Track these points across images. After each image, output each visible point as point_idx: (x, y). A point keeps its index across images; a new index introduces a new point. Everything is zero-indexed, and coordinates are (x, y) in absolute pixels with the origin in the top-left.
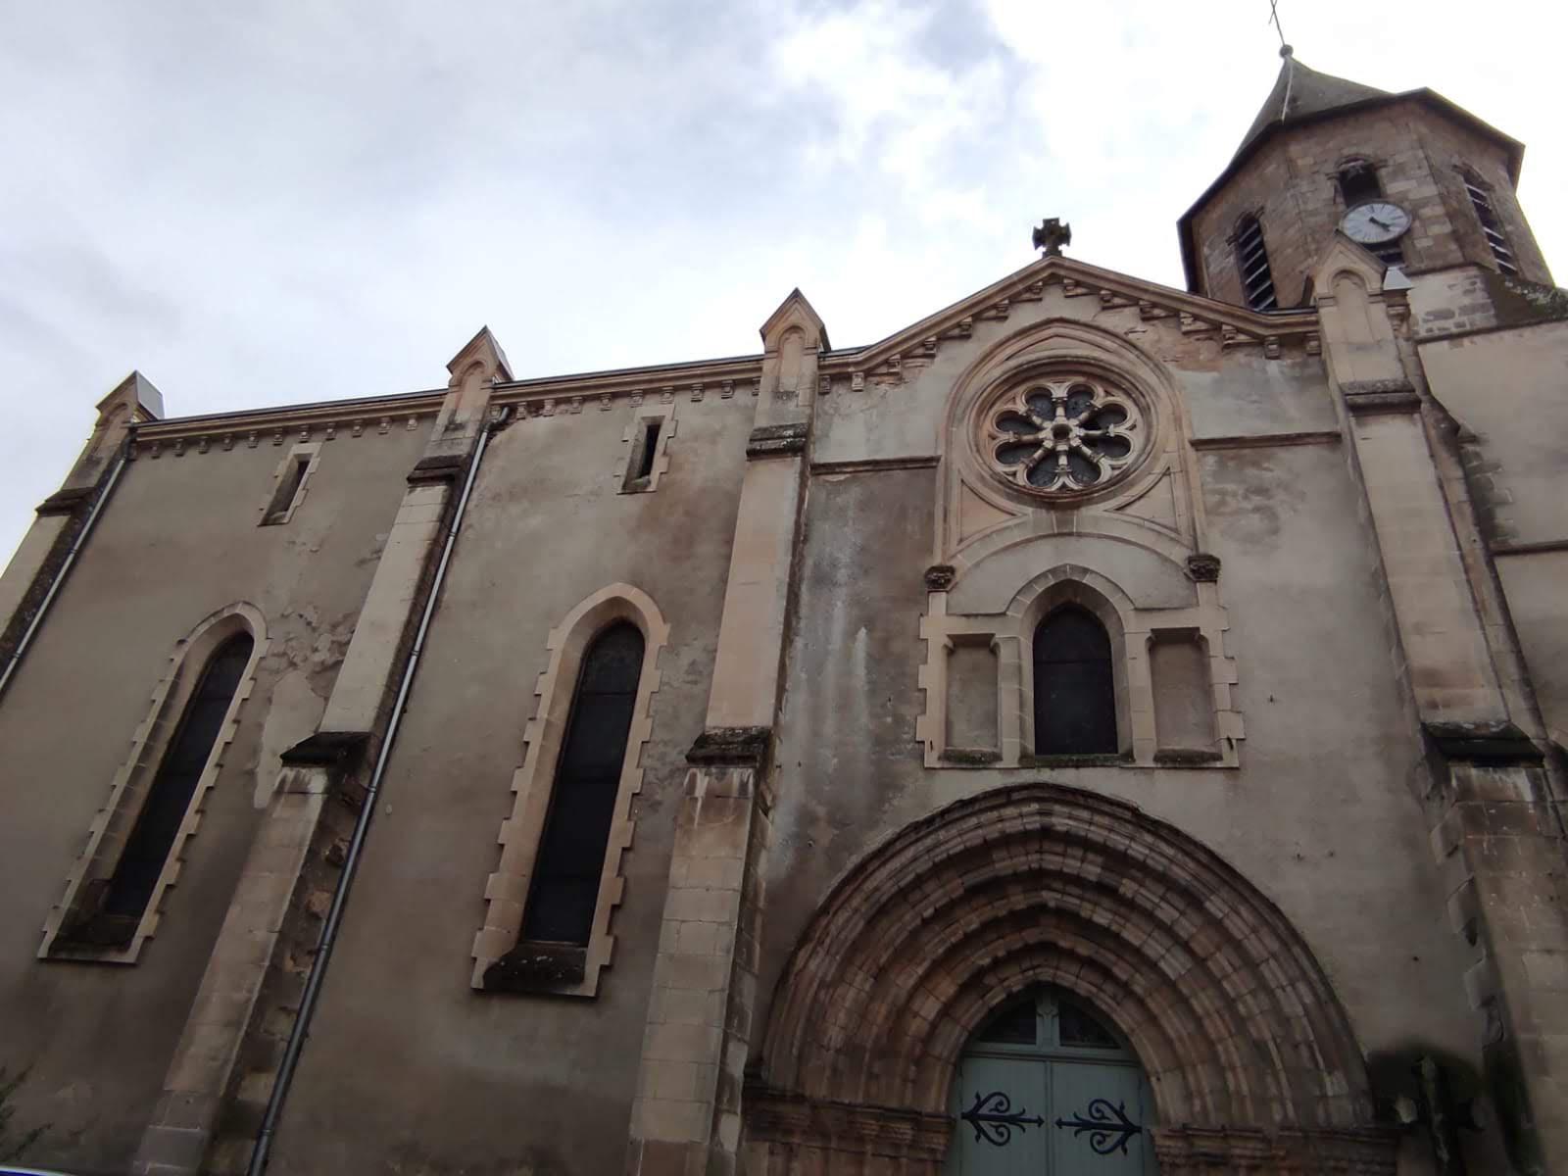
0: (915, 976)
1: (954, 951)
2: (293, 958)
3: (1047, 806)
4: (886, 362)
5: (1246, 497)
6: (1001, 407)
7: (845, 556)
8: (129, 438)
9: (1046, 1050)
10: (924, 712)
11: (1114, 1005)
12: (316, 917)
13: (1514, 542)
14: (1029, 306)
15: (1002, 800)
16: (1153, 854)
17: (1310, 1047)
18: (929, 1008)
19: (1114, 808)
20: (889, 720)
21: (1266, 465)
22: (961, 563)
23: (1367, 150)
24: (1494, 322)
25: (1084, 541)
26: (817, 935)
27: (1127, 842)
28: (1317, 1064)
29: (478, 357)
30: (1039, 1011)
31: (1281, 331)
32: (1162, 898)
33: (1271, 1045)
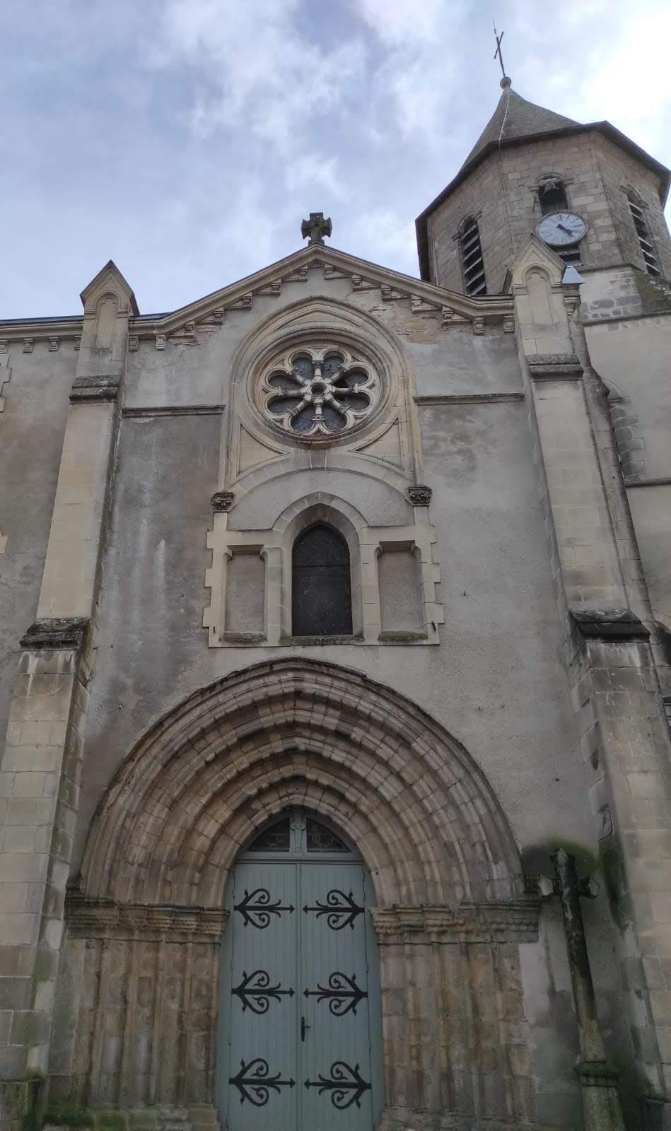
3: (299, 675)
4: (184, 327)
6: (273, 367)
7: (149, 484)
9: (298, 855)
11: (346, 820)
13: (643, 478)
14: (297, 285)
15: (266, 670)
16: (376, 709)
17: (483, 845)
18: (210, 828)
23: (559, 170)
24: (639, 312)
32: (382, 741)
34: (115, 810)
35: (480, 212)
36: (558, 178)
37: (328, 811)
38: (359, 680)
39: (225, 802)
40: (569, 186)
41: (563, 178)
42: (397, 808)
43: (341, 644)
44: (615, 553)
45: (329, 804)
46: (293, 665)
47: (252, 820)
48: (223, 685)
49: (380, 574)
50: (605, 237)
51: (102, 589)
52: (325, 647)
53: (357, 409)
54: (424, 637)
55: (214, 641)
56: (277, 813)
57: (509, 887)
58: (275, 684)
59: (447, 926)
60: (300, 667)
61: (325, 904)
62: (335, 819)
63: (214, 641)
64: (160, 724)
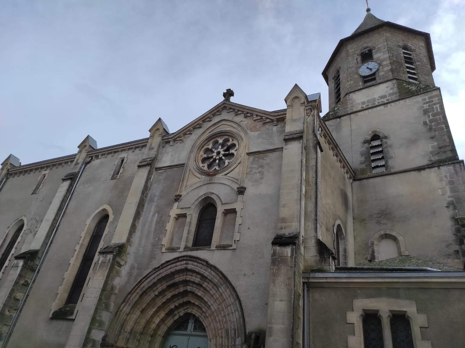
0: (153, 311)
1: (164, 304)
2: (9, 311)
3: (187, 262)
4: (179, 137)
5: (257, 169)
6: (205, 147)
7: (157, 194)
8: (7, 173)
10: (165, 236)
11: (204, 319)
12: (18, 300)
13: (393, 171)
14: (218, 116)
15: (177, 260)
16: (210, 275)
18: (157, 320)
19: (202, 262)
20: (157, 239)
21: (265, 159)
22: (183, 194)
23: (370, 45)
24: (398, 98)
25: (215, 185)
26: (127, 300)
27: (204, 271)
28: (235, 335)
29: (86, 144)
30: (189, 322)
31: (277, 117)
34: (122, 312)
35: (340, 67)
36: (370, 48)
38: (205, 264)
39: (164, 311)
40: (373, 50)
41: (371, 47)
43: (203, 250)
44: (299, 209)
45: (199, 313)
46: (185, 258)
48: (163, 266)
49: (224, 222)
50: (386, 69)
51: (136, 232)
52: (198, 251)
53: (229, 159)
54: (231, 246)
55: (164, 250)
56: (183, 316)
58: (179, 265)
60: (187, 259)
63: (164, 250)
64: (141, 281)
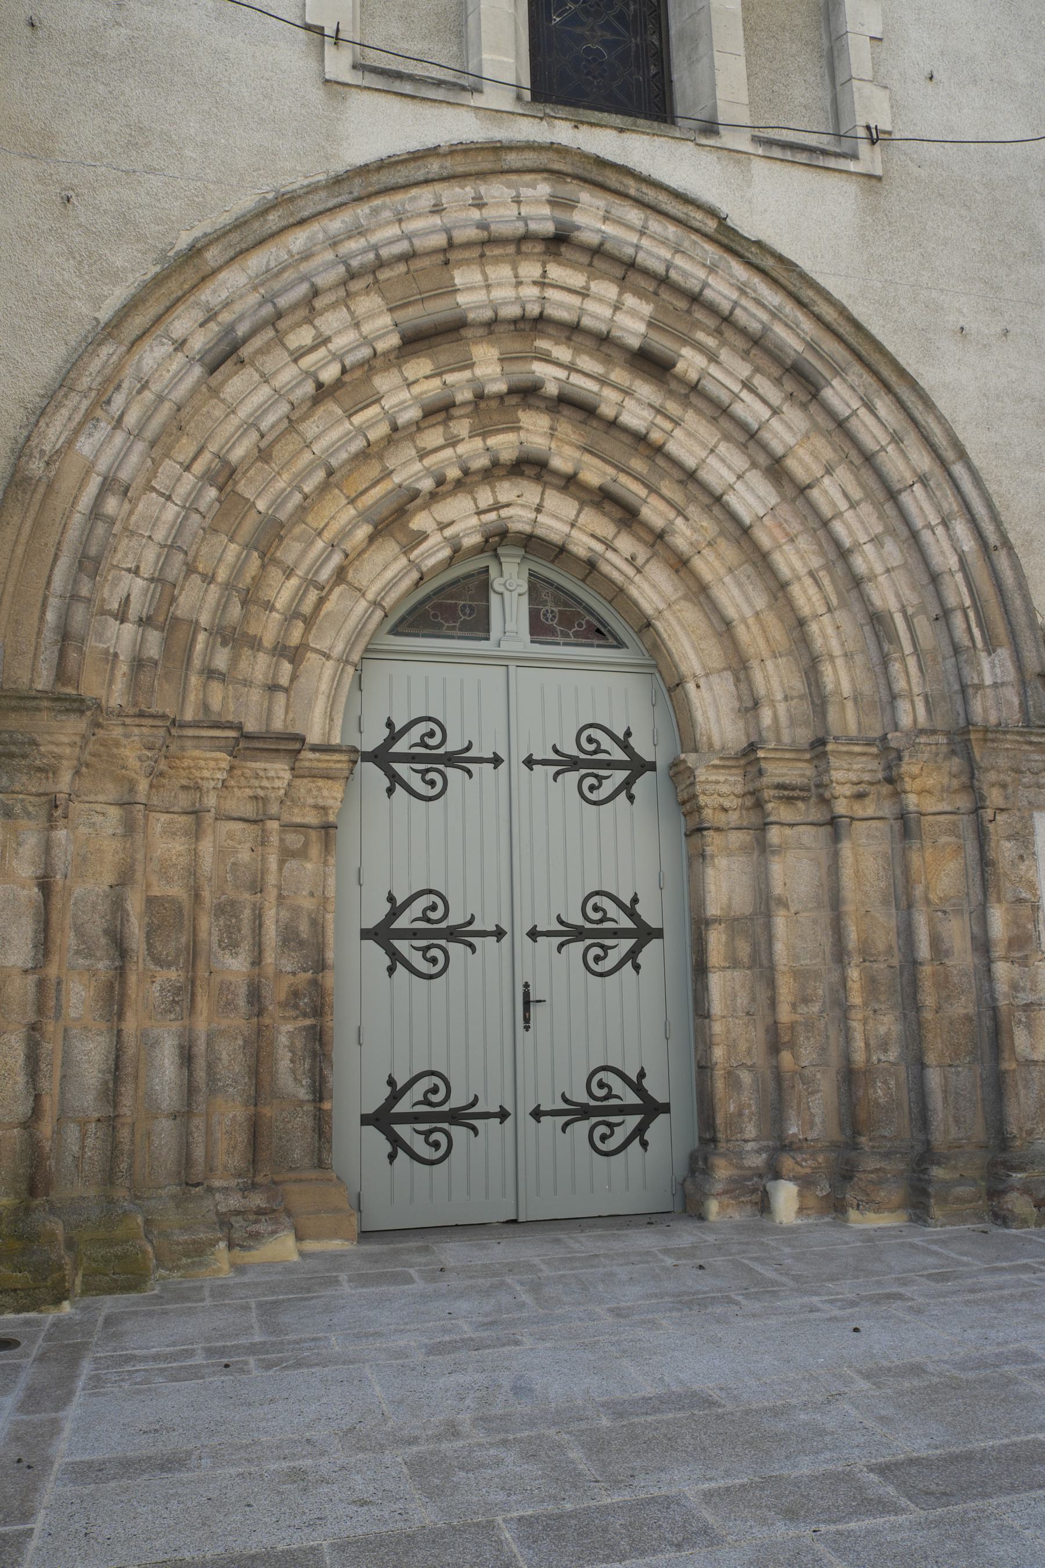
9: (509, 647)
11: (630, 571)
15: (485, 163)
17: (964, 611)
32: (747, 385)
33: (898, 618)
37: (590, 549)
42: (765, 540)
45: (593, 536)
47: (412, 557)
52: (625, 135)
57: (1016, 701)
59: (871, 784)
61: (574, 751)
62: (606, 568)
